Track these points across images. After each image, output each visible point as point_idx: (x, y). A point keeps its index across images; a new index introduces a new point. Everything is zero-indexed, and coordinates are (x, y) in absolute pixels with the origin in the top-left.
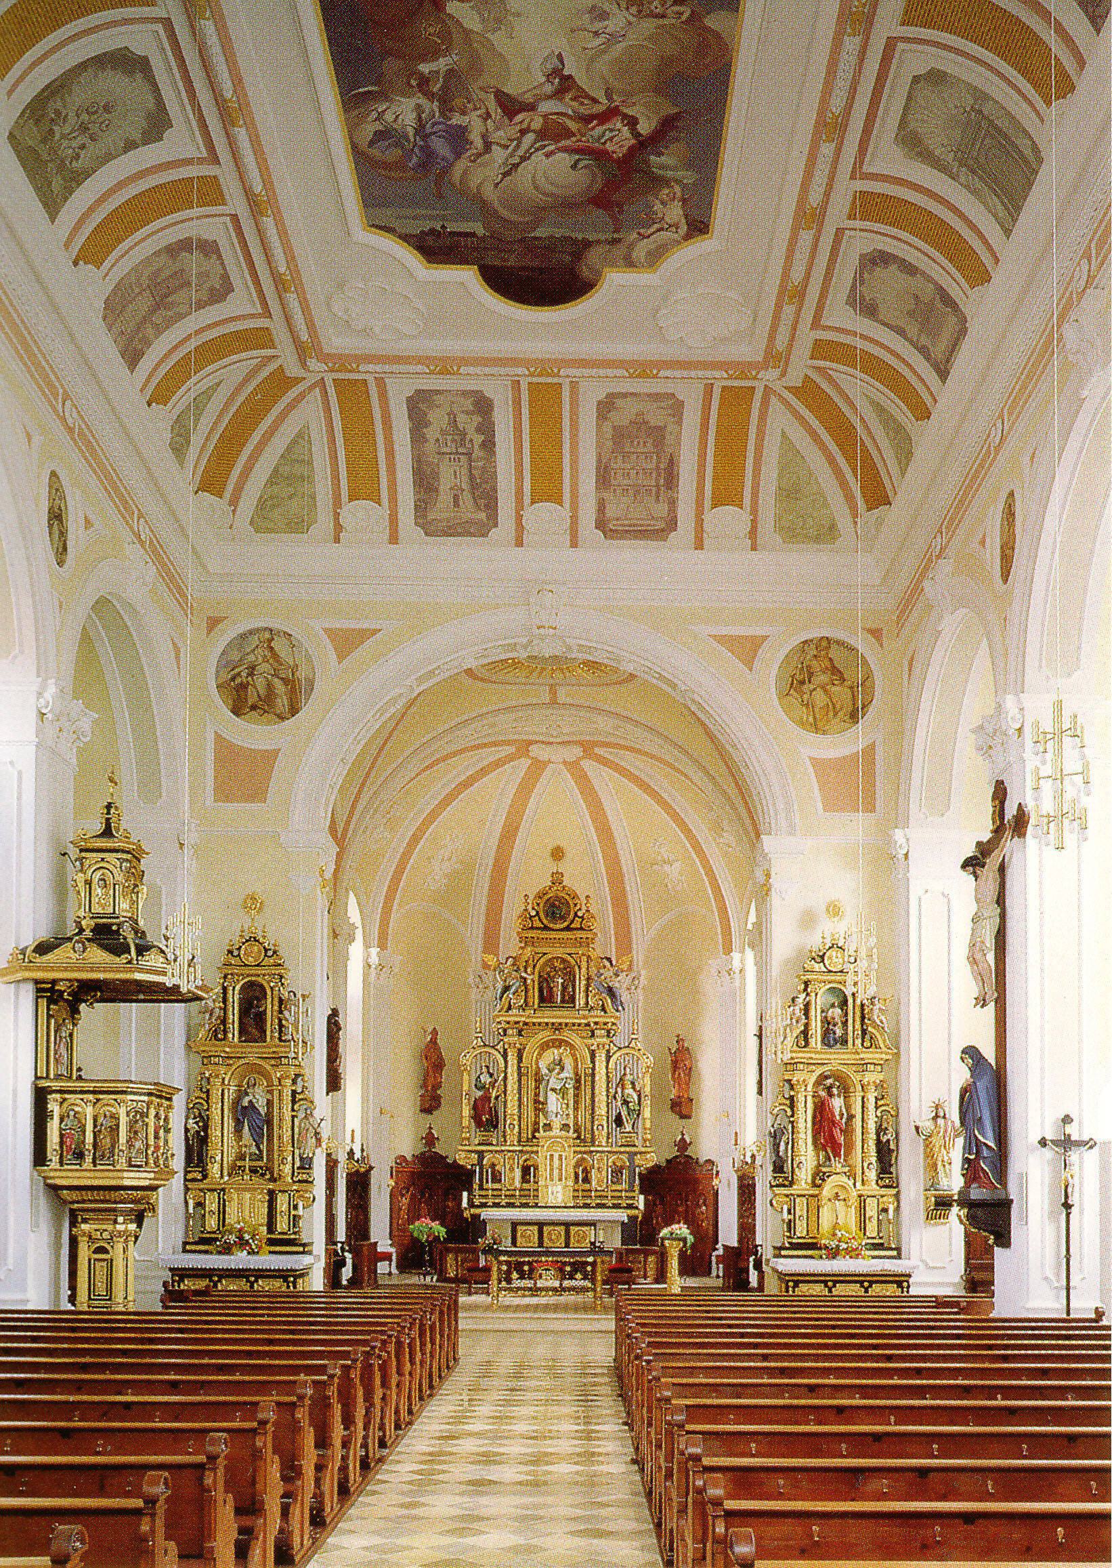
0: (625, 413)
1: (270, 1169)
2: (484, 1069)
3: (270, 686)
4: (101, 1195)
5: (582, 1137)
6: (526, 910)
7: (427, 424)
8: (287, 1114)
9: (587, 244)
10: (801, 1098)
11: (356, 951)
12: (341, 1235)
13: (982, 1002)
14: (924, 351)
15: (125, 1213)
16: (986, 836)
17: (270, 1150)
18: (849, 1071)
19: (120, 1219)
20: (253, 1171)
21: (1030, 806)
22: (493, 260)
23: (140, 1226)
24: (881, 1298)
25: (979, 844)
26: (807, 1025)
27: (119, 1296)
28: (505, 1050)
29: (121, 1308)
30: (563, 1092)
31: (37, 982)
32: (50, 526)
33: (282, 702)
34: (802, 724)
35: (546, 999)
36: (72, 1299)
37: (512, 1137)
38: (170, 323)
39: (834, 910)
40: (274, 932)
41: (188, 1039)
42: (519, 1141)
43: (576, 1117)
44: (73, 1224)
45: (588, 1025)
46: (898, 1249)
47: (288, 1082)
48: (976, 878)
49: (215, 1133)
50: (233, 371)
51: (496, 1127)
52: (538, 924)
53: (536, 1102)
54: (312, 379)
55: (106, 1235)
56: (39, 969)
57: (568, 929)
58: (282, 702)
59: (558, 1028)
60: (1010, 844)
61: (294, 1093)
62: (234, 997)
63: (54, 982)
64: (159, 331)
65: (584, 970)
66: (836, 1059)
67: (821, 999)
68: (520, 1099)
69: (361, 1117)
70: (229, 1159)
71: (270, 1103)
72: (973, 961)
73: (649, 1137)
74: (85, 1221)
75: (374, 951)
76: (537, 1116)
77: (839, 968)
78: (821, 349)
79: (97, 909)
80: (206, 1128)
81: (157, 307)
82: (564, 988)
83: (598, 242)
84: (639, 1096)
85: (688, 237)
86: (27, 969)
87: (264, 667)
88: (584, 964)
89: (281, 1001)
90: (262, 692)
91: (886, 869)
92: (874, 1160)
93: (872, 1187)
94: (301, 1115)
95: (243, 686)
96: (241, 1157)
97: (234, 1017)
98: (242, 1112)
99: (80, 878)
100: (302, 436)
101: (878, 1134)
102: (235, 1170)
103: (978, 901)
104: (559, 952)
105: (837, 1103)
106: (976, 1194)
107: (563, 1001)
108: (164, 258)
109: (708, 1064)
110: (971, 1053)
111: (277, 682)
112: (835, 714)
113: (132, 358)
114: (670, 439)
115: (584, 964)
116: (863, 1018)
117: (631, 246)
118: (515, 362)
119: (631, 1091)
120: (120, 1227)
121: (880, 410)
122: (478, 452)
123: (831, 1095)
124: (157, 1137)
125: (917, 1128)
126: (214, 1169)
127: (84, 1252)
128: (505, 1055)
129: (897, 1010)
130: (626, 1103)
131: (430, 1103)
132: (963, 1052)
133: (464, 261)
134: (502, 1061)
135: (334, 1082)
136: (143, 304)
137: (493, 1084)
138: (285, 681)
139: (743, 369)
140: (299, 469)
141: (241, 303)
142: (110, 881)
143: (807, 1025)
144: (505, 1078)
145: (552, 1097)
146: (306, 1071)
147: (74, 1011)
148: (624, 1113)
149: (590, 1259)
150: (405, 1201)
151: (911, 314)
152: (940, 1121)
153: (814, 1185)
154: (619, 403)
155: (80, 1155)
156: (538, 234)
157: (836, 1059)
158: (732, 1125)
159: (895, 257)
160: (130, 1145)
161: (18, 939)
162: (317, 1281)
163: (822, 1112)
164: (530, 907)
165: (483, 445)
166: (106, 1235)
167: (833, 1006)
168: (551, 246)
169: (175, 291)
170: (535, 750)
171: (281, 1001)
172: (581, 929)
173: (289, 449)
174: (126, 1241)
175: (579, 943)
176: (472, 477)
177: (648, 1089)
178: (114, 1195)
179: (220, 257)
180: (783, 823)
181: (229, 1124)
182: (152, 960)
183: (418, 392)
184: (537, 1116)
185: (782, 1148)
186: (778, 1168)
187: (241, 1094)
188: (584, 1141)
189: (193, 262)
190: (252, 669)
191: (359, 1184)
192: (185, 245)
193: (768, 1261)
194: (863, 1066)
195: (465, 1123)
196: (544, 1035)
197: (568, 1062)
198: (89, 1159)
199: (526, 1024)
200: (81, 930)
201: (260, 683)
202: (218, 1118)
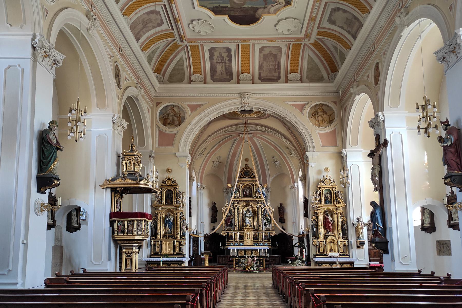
0: (266, 52)
1: (173, 235)
3: (173, 119)
4: (129, 242)
5: (255, 228)
7: (214, 55)
8: (179, 222)
9: (258, 9)
10: (320, 216)
11: (194, 183)
12: (191, 253)
13: (376, 190)
14: (349, 32)
15: (136, 247)
16: (374, 148)
17: (174, 231)
18: (333, 210)
19: (134, 248)
20: (169, 236)
21: (388, 138)
22: (232, 13)
23: (139, 250)
24: (324, 269)
25: (371, 150)
26: (320, 198)
27: (134, 268)
29: (134, 271)
30: (250, 217)
31: (111, 188)
32: (116, 78)
33: (176, 122)
34: (315, 124)
35: (245, 195)
36: (120, 269)
37: (236, 230)
38: (147, 31)
39: (326, 170)
40: (175, 176)
41: (152, 204)
42: (238, 229)
43: (253, 223)
44: (121, 249)
46: (349, 255)
47: (179, 214)
48: (372, 158)
49: (159, 227)
50: (161, 44)
52: (242, 177)
53: (242, 220)
54: (185, 44)
55: (130, 252)
56: (112, 184)
57: (250, 178)
58: (176, 122)
59: (248, 202)
60: (382, 149)
61: (180, 217)
62: (164, 193)
63: (117, 188)
64: (144, 33)
65: (255, 188)
66: (329, 207)
67: (324, 192)
69: (198, 222)
70: (163, 232)
71: (174, 220)
72: (372, 179)
74: (125, 249)
75: (199, 184)
76: (243, 223)
77: (329, 184)
78: (319, 33)
79: (128, 170)
80: (157, 225)
81: (143, 28)
82: (249, 192)
83: (261, 8)
85: (285, 6)
86: (109, 184)
87: (172, 114)
88: (255, 186)
89: (177, 194)
90: (171, 120)
91: (341, 159)
92: (341, 232)
93: (341, 239)
94: (182, 222)
95: (166, 119)
96: (166, 233)
97: (164, 198)
98: (166, 222)
99: (124, 162)
100: (181, 59)
101: (342, 226)
102: (164, 236)
103: (373, 164)
104: (248, 183)
105: (330, 218)
106: (377, 239)
108: (146, 15)
109: (289, 211)
110: (373, 204)
111: (175, 118)
112: (325, 122)
113: (138, 40)
114: (278, 57)
115: (255, 186)
116: (336, 196)
117: (269, 9)
118: (238, 39)
119: (268, 217)
120: (134, 250)
121: (336, 48)
122: (227, 62)
123: (328, 216)
124: (145, 226)
125: (353, 224)
126: (159, 236)
127: (124, 257)
128: (234, 208)
129: (345, 194)
130: (267, 220)
131: (214, 220)
132: (371, 203)
133: (225, 14)
134: (233, 210)
135: (190, 215)
136: (140, 26)
137: (231, 216)
138: (177, 117)
139: (298, 39)
140: (180, 67)
141: (165, 26)
142: (132, 162)
143: (320, 198)
144: (234, 214)
145: (247, 219)
146: (184, 211)
147: (122, 197)
148: (266, 222)
150: (208, 245)
151: (345, 23)
152: (360, 222)
153: (324, 239)
154: (265, 49)
155: (123, 232)
156: (244, 6)
157: (329, 207)
158: (297, 225)
159: (341, 8)
160: (137, 229)
161: (106, 177)
162: (186, 264)
163: (325, 220)
165: (229, 60)
166: (130, 252)
167: (327, 193)
168: (248, 9)
169: (148, 23)
170: (241, 135)
171: (177, 194)
173: (178, 62)
174: (136, 254)
175: (253, 181)
176: (225, 68)
178: (132, 242)
179: (160, 15)
180: (311, 148)
181: (163, 225)
182: (144, 182)
183: (212, 48)
184: (243, 223)
185: (315, 229)
186: (314, 234)
187: (166, 216)
188: (256, 229)
189: (153, 16)
190: (168, 115)
191: (196, 241)
192: (152, 12)
193: (312, 259)
194: (337, 209)
196: (244, 204)
197: (251, 210)
198: (126, 232)
200: (124, 175)
201: (171, 118)
202: (160, 223)
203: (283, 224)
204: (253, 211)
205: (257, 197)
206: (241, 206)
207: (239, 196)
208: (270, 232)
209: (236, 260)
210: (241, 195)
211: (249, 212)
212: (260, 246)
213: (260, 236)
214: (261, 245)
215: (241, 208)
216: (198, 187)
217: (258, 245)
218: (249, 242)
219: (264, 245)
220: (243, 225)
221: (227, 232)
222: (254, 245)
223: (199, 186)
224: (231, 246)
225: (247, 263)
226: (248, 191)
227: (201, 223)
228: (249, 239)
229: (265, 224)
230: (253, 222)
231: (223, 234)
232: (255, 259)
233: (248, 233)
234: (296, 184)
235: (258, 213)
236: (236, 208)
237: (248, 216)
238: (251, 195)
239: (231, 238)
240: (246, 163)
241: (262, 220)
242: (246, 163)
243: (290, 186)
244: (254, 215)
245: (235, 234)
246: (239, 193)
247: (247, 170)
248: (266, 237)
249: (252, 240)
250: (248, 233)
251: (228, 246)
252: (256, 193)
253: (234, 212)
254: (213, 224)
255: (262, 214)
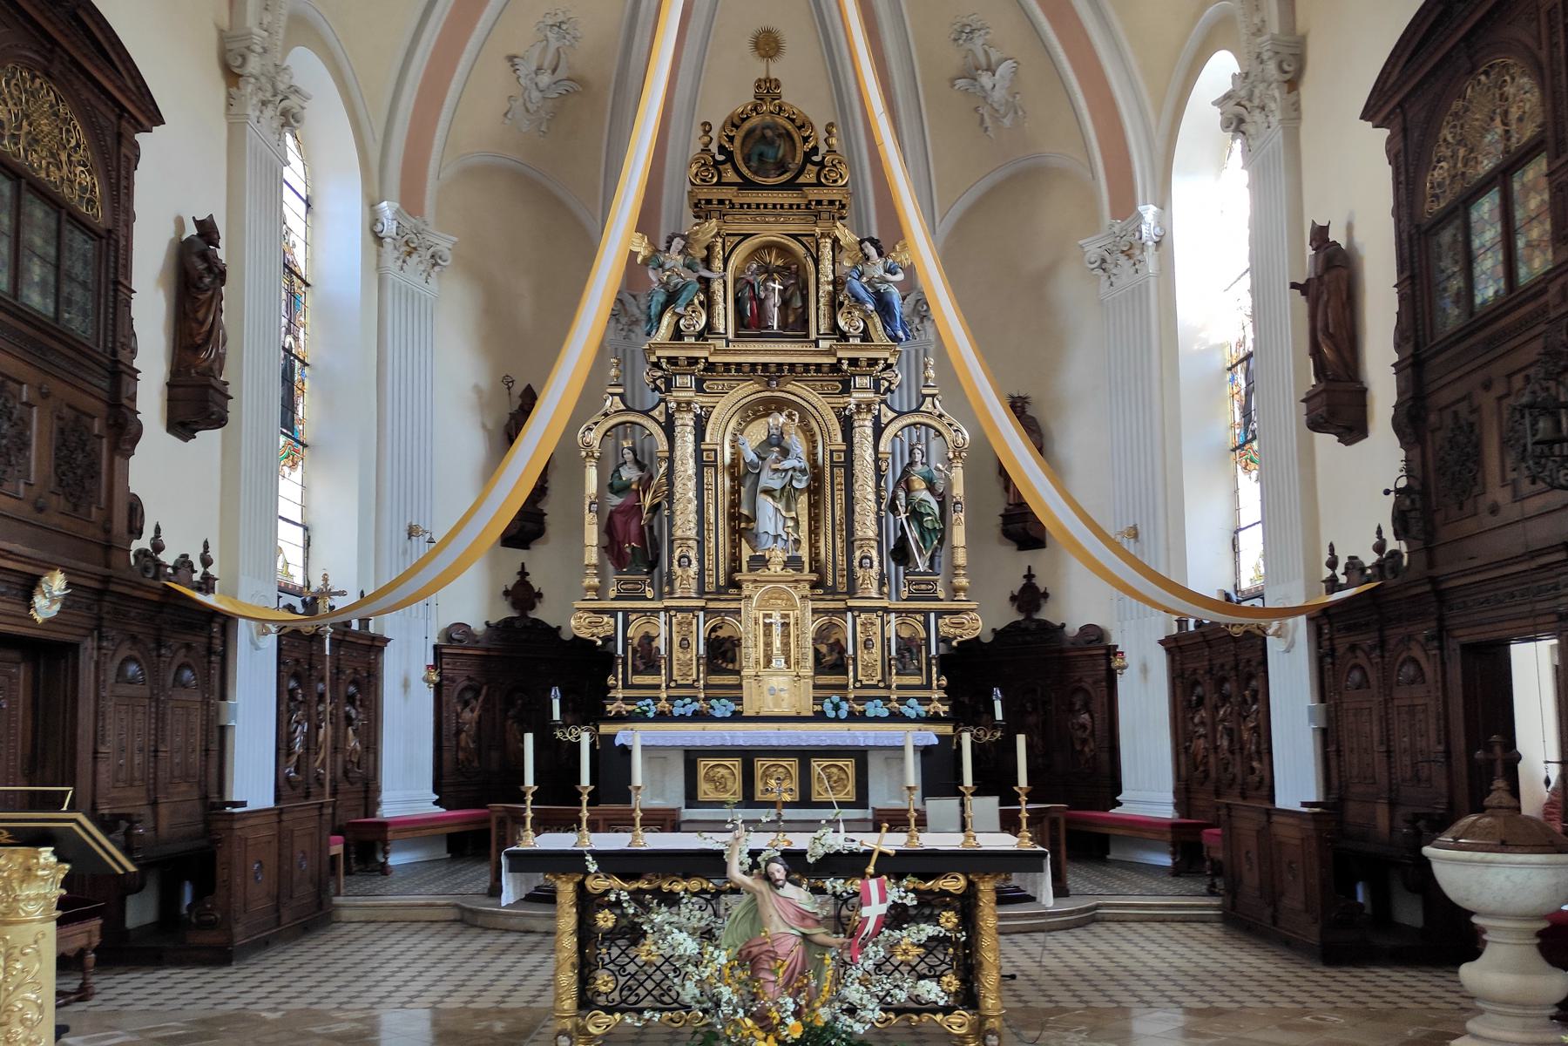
2: (629, 456)
5: (829, 584)
6: (706, 150)
28: (670, 418)
30: (787, 495)
35: (750, 323)
42: (701, 592)
43: (813, 546)
45: (835, 368)
51: (654, 564)
53: (734, 517)
57: (791, 185)
59: (771, 373)
68: (701, 511)
73: (963, 582)
76: (735, 545)
82: (785, 304)
84: (942, 504)
104: (772, 232)
107: (784, 324)
119: (924, 495)
128: (669, 428)
130: (916, 515)
134: (662, 444)
137: (645, 484)
145: (766, 506)
148: (913, 534)
149: (954, 884)
164: (714, 148)
172: (819, 184)
175: (814, 211)
177: (958, 491)
184: (735, 545)
188: (832, 591)
195: (592, 556)
196: (746, 391)
197: (798, 444)
199: (710, 367)
203: (1028, 558)
204: (812, 454)
205: (844, 336)
206: (726, 404)
207: (709, 327)
208: (940, 614)
209: (587, 903)
210: (724, 320)
211: (785, 453)
212: (861, 718)
213: (867, 645)
214: (872, 709)
215: (731, 430)
216: (379, 239)
217: (853, 717)
218: (777, 686)
219: (896, 717)
220: (735, 559)
221: (612, 613)
222: (820, 717)
223: (389, 227)
224: (641, 717)
225: (750, 960)
226: (780, 298)
227: (412, 532)
228: (778, 662)
229: (901, 553)
230: (814, 531)
231: (578, 625)
232: (874, 911)
233: (776, 629)
234: (1149, 212)
235: (848, 463)
236: (685, 422)
237: (776, 483)
238: (796, 325)
239: (647, 658)
240: (759, 69)
241: (879, 520)
242: (759, 69)
243: (1093, 248)
244: (821, 485)
245: (680, 638)
246: (709, 305)
247: (773, 126)
248: (908, 647)
249: (808, 669)
250: (776, 618)
251: (619, 718)
252: (835, 306)
253: (671, 460)
254: (517, 556)
255: (879, 475)
